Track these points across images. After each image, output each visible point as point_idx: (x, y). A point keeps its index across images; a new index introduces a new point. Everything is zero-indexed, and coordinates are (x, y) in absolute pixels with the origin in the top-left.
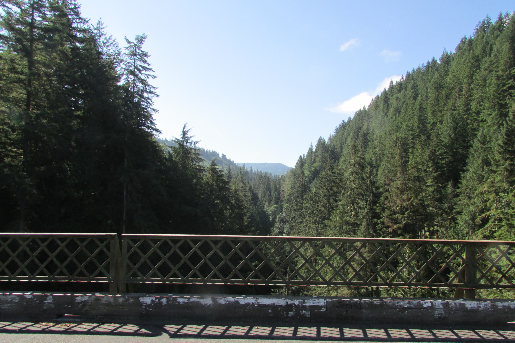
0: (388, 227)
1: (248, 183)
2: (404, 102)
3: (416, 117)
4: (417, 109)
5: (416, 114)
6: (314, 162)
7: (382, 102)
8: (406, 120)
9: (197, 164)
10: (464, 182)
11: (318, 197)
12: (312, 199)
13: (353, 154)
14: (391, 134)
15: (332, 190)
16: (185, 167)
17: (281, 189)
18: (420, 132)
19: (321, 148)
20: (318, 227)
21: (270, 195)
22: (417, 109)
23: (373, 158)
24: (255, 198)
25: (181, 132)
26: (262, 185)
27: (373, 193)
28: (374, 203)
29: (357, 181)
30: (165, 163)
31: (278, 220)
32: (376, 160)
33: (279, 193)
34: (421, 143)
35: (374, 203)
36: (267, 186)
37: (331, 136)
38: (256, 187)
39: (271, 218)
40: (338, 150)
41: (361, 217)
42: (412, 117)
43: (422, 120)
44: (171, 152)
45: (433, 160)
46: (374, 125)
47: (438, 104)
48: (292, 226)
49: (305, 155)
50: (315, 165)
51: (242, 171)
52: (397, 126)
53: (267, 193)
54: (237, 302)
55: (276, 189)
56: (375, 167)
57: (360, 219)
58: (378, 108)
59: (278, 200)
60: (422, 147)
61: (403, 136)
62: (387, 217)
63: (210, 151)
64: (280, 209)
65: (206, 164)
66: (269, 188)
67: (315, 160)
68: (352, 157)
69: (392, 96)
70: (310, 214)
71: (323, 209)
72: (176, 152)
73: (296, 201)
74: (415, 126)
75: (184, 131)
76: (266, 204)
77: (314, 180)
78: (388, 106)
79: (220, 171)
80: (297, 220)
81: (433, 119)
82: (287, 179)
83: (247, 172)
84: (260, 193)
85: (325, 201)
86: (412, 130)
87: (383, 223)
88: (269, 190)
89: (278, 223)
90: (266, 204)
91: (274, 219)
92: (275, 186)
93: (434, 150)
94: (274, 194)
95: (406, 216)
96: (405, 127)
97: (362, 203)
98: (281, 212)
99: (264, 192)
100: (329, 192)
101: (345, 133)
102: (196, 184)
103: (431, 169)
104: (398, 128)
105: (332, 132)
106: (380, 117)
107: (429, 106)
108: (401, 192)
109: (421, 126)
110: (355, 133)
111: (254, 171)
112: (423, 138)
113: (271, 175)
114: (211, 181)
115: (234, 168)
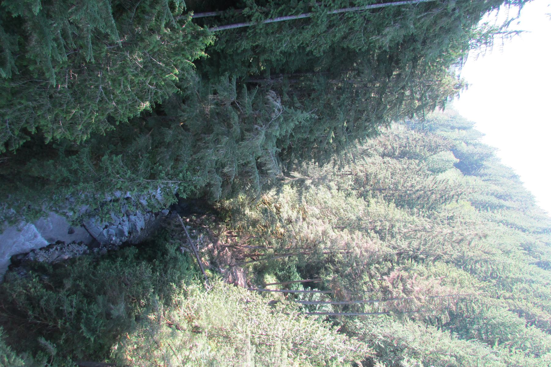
5: (525, 275)
6: (467, 143)
10: (439, 333)
15: (432, 193)
40: (482, 171)
42: (521, 270)
47: (536, 297)
48: (388, 136)
50: (463, 144)
54: (64, 339)
67: (471, 143)
71: (409, 184)
73: (419, 139)
75: (520, 32)
96: (508, 262)
100: (430, 191)
104: (507, 253)
109: (509, 280)
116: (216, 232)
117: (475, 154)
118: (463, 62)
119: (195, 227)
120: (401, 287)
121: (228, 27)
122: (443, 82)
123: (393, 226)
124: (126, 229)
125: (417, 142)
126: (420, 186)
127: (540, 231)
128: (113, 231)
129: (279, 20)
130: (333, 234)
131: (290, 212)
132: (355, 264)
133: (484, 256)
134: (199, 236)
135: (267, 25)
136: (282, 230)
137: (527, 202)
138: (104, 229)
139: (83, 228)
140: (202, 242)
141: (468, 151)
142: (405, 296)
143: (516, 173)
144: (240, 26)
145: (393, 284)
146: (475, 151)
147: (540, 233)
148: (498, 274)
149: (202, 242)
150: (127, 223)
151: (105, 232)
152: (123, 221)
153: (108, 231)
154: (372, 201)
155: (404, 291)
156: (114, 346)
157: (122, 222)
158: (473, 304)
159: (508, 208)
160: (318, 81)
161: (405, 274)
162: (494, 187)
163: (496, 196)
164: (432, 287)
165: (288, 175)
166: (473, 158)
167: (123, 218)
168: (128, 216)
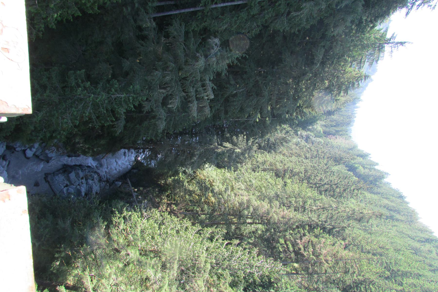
2: (426, 258)
3: (410, 270)
4: (418, 271)
5: (413, 269)
6: (364, 167)
7: (427, 237)
8: (406, 259)
9: (366, 61)
11: (330, 175)
13: (374, 212)
15: (337, 187)
16: (364, 47)
18: (393, 270)
19: (378, 174)
20: (302, 174)
21: (332, 126)
22: (418, 271)
25: (403, 41)
26: (342, 118)
27: (334, 228)
28: (324, 229)
29: (345, 214)
30: (369, 26)
31: (308, 134)
33: (334, 135)
34: (382, 273)
35: (324, 229)
36: (341, 123)
39: (310, 127)
40: (376, 190)
42: (409, 266)
43: (405, 274)
44: (382, 31)
45: (364, 281)
46: (402, 226)
48: (303, 148)
50: (361, 168)
53: (334, 124)
55: (337, 132)
57: (308, 215)
58: (420, 232)
59: (327, 134)
60: (377, 273)
61: (390, 255)
62: (310, 239)
64: (318, 135)
65: (365, 69)
66: (339, 125)
67: (367, 168)
68: (369, 212)
69: (434, 247)
70: (314, 167)
71: (318, 178)
72: (381, 36)
74: (400, 268)
75: (405, 43)
77: (346, 167)
78: (422, 242)
79: (359, 84)
80: (309, 152)
81: (406, 283)
82: (347, 141)
83: (355, 104)
85: (326, 181)
86: (396, 263)
87: (304, 235)
88: (337, 125)
89: (305, 133)
90: (324, 123)
92: (341, 131)
93: (375, 283)
94: (332, 130)
97: (323, 218)
98: (316, 136)
99: (335, 120)
100: (335, 185)
101: (394, 198)
102: (346, 61)
103: (355, 277)
104: (397, 250)
105: (394, 186)
106: (410, 233)
107: (421, 282)
110: (394, 207)
111: (355, 109)
112: (388, 273)
113: (352, 126)
114: (347, 76)
115: (360, 91)
116: (157, 200)
117: (371, 176)
118: (362, 65)
119: (141, 194)
120: (311, 249)
121: (183, 11)
122: (346, 71)
123: (305, 202)
124: (83, 190)
125: (325, 154)
126: (328, 180)
127: (424, 240)
128: (72, 190)
129: (222, 5)
130: (256, 203)
131: (221, 186)
132: (273, 230)
133: (379, 250)
134: (143, 202)
135: (213, 9)
136: (213, 199)
137: (411, 217)
138: (64, 187)
139: (47, 185)
140: (146, 206)
141: (364, 173)
142: (315, 258)
143: (404, 194)
144: (192, 10)
145: (304, 247)
146: (370, 173)
147: (424, 242)
148: (391, 267)
149: (146, 206)
150: (85, 185)
151: (65, 190)
152: (82, 183)
153: (68, 190)
154: (289, 181)
155: (313, 254)
156: (56, 262)
157: (81, 184)
158: (371, 286)
159: (397, 220)
160: (249, 66)
161: (315, 240)
162: (386, 202)
163: (387, 209)
164: (337, 252)
165: (221, 145)
166: (368, 179)
167: (82, 180)
168: (86, 180)
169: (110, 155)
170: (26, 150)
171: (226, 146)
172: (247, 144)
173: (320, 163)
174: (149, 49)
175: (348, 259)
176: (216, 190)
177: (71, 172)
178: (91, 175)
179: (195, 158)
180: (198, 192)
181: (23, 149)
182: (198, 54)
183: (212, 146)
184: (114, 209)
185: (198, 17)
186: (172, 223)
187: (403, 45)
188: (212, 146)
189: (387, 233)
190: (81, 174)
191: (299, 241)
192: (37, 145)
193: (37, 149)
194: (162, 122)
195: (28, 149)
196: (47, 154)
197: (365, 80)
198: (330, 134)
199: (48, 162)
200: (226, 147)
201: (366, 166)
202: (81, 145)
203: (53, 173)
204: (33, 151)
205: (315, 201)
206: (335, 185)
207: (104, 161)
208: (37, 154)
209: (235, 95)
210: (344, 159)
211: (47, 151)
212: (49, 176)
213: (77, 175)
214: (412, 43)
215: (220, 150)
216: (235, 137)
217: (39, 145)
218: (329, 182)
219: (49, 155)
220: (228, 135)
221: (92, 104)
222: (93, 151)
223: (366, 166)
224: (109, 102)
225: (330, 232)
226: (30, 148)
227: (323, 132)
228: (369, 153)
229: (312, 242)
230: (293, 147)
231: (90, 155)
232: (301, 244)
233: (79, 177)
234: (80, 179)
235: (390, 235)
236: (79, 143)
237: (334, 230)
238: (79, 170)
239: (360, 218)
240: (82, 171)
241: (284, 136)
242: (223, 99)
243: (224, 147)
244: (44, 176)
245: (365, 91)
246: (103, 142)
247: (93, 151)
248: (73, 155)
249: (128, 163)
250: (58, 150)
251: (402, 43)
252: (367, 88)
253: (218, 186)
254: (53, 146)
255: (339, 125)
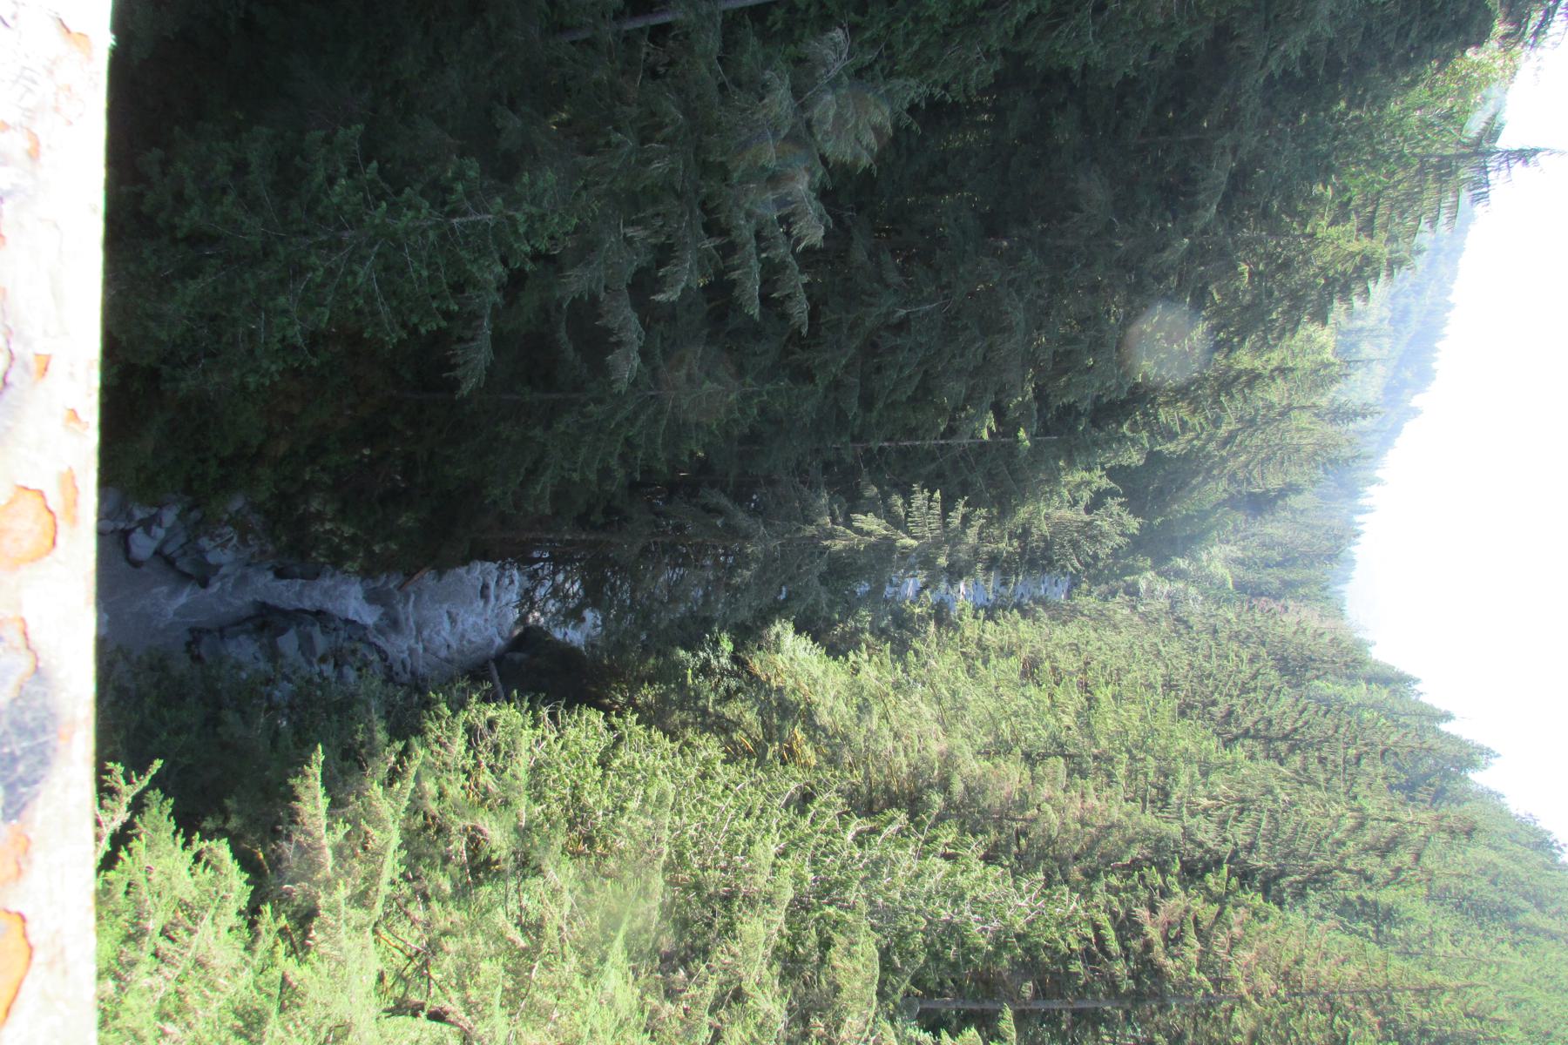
0: (1153, 909)
1: (1313, 483)
11: (1265, 700)
12: (1254, 677)
14: (1515, 1005)
17: (1290, 603)
19: (1449, 750)
21: (1268, 566)
23: (1413, 927)
24: (1260, 504)
25: (1528, 145)
26: (1305, 536)
28: (1246, 876)
32: (1407, 942)
37: (1499, 796)
38: (1301, 519)
39: (1182, 563)
41: (1190, 822)
49: (1422, 699)
51: (1362, 463)
52: (1548, 1034)
55: (1288, 585)
56: (1378, 932)
57: (1180, 818)
62: (1187, 911)
63: (1436, 359)
66: (1295, 560)
75: (1535, 152)
76: (1234, 551)
83: (1354, 494)
84: (1274, 528)
85: (1247, 722)
87: (1165, 893)
90: (1234, 551)
91: (1180, 574)
92: (1302, 583)
94: (1272, 578)
95: (1194, 974)
100: (1285, 737)
101: (1517, 848)
105: (1517, 804)
108: (1287, 974)
111: (1357, 518)
167: (324, 667)
169: (427, 578)
170: (132, 530)
171: (866, 527)
172: (946, 525)
173: (1227, 657)
174: (595, 76)
175: (1342, 992)
176: (823, 718)
177: (284, 631)
178: (354, 652)
179: (747, 573)
180: (757, 730)
181: (121, 525)
182: (768, 74)
183: (810, 530)
184: (432, 694)
185: (774, 24)
186: (648, 752)
187: (1526, 162)
188: (810, 530)
189: (1493, 970)
190: (321, 643)
191: (1142, 913)
192: (169, 516)
193: (168, 530)
194: (627, 357)
195: (139, 530)
196: (202, 552)
197: (1390, 275)
198: (1262, 594)
199: (204, 583)
200: (869, 534)
201: (1402, 720)
202: (328, 526)
203: (221, 630)
204: (153, 538)
205: (1205, 774)
206: (1285, 737)
207: (408, 612)
208: (168, 550)
209: (902, 326)
210: (1317, 665)
211: (205, 542)
212: (206, 639)
213: (306, 645)
214: (1562, 153)
215: (839, 545)
216: (897, 500)
217: (179, 517)
218: (1261, 726)
219: (212, 558)
220: (873, 491)
221: (378, 255)
222: (370, 554)
223: (1402, 720)
224: (443, 237)
225: (1269, 885)
226: (147, 525)
227: (1236, 586)
228: (1415, 675)
229: (1195, 919)
230: (1119, 617)
231: (356, 566)
232: (1155, 925)
233: (313, 652)
234: (315, 660)
235: (1504, 976)
236: (319, 517)
237: (1284, 882)
238: (313, 625)
239: (1387, 844)
240: (323, 632)
241: (1087, 518)
242: (857, 342)
243: (859, 531)
244: (188, 638)
245: (1390, 452)
246: (406, 520)
247: (370, 554)
248: (297, 570)
249: (492, 631)
250: (243, 540)
251: (1524, 155)
252: (1398, 442)
253: (833, 709)
254: (227, 523)
255: (1295, 560)
